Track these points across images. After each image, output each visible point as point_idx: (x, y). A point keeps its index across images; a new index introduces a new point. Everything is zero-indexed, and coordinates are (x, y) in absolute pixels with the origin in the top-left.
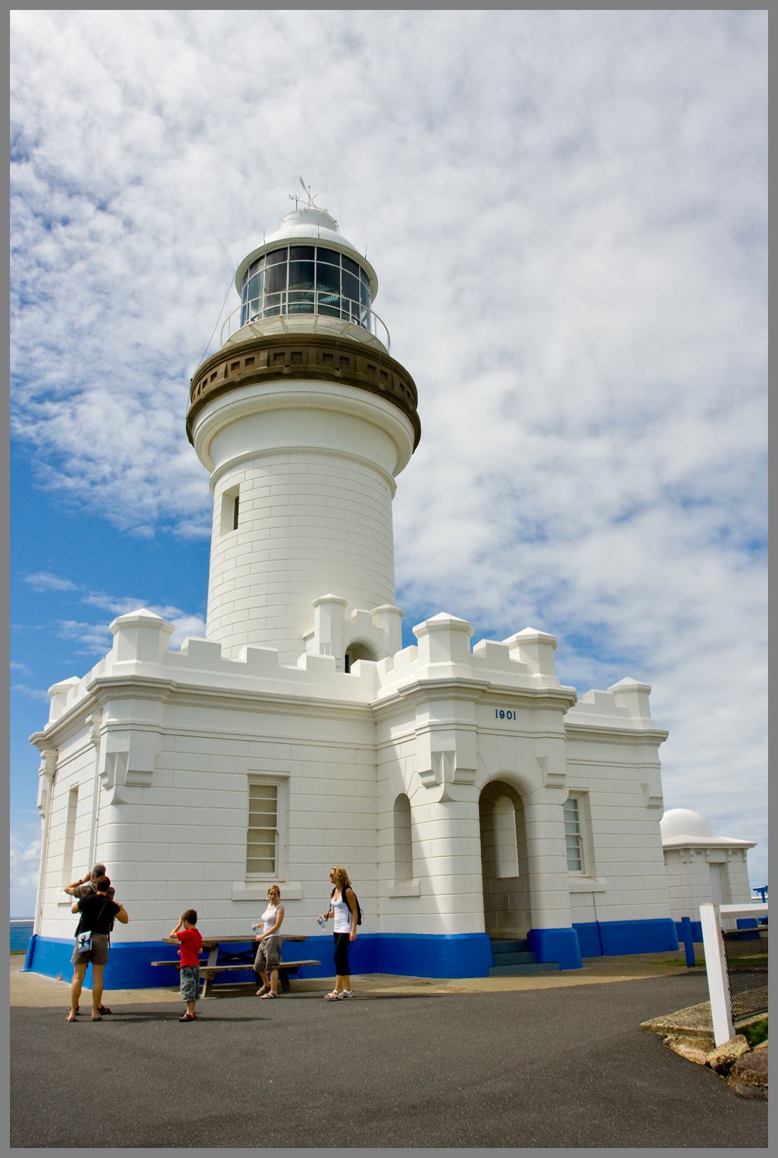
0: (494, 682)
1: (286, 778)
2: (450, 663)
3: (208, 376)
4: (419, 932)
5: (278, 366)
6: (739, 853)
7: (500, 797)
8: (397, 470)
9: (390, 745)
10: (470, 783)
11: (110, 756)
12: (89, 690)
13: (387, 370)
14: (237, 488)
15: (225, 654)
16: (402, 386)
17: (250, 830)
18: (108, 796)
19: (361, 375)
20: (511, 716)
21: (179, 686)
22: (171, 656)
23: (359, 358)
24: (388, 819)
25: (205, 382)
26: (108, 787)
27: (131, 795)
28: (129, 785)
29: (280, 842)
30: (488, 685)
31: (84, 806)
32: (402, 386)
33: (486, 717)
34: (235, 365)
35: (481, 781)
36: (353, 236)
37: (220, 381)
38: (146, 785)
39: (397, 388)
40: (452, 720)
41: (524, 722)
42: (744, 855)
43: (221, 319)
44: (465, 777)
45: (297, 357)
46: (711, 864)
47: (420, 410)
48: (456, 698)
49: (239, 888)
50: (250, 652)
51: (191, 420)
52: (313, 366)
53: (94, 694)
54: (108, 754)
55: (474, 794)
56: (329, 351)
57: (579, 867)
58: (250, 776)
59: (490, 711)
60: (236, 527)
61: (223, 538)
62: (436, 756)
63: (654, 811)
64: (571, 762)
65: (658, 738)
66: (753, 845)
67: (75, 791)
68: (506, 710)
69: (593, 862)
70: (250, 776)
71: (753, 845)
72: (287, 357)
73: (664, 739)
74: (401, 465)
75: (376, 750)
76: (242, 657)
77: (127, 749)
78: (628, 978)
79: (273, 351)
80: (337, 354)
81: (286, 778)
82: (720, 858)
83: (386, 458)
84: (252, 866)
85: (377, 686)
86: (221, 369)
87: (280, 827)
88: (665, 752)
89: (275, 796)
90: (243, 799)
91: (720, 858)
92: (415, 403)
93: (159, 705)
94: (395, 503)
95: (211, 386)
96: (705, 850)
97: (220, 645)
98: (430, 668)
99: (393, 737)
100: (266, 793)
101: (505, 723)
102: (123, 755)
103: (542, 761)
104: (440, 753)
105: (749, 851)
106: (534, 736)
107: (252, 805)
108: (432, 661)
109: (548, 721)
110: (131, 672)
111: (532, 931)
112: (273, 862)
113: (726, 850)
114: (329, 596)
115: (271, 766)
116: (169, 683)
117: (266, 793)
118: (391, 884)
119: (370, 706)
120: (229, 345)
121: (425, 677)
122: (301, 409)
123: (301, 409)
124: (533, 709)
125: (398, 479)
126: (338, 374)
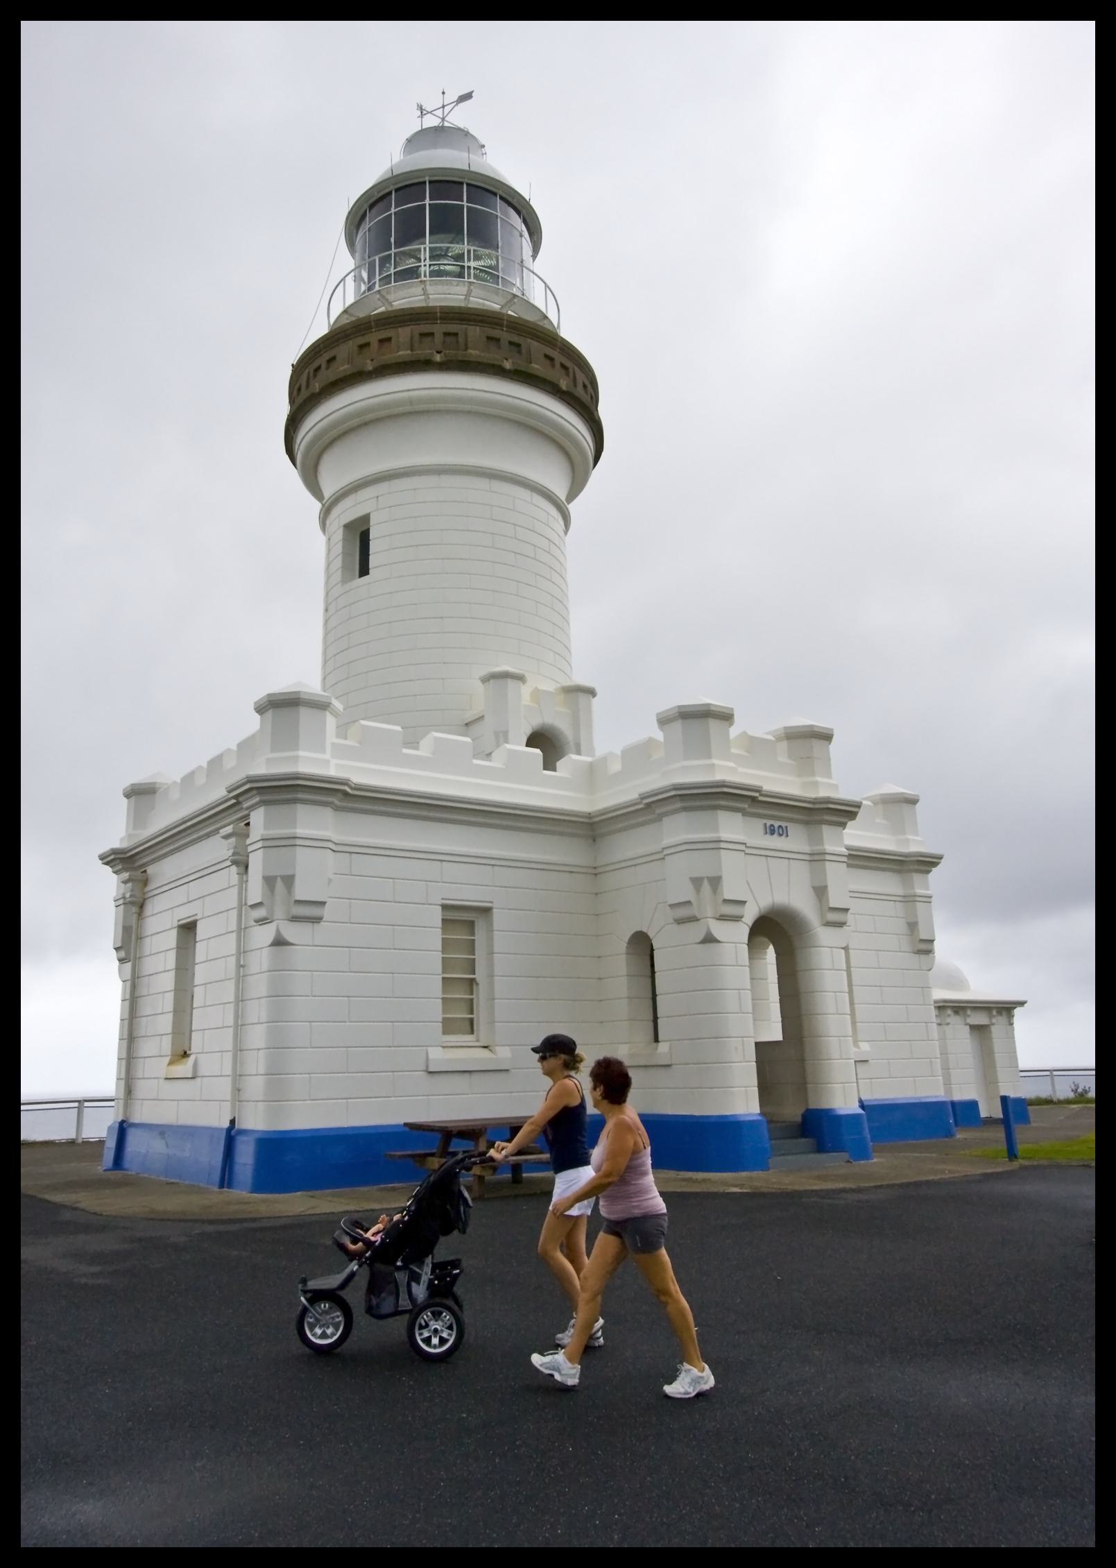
0: (767, 787)
1: (486, 911)
3: (322, 361)
5: (423, 352)
6: (1004, 1013)
8: (573, 493)
10: (737, 918)
12: (229, 792)
13: (568, 364)
14: (365, 519)
16: (585, 386)
17: (443, 978)
19: (537, 368)
20: (782, 832)
21: (359, 788)
24: (619, 964)
25: (317, 369)
26: (262, 921)
30: (758, 790)
31: (214, 947)
32: (585, 386)
35: (750, 914)
39: (566, 376)
42: (1010, 1016)
43: (322, 285)
45: (449, 339)
47: (605, 411)
48: (685, 809)
49: (437, 1056)
52: (474, 353)
53: (236, 797)
55: (743, 931)
56: (425, 328)
57: (471, 1027)
59: (758, 824)
60: (364, 570)
61: (348, 586)
63: (923, 957)
64: (856, 895)
65: (927, 863)
66: (1022, 1004)
67: (188, 929)
68: (777, 824)
69: (492, 1022)
71: (1022, 1004)
72: (439, 338)
73: (935, 864)
75: (595, 872)
78: (534, 1175)
80: (505, 336)
81: (941, 858)
82: (980, 1019)
83: (555, 479)
84: (449, 1026)
87: (480, 975)
89: (473, 934)
90: (435, 937)
91: (980, 1019)
92: (595, 399)
95: (328, 375)
96: (964, 1008)
101: (775, 842)
105: (1017, 1012)
107: (446, 945)
108: (273, 750)
111: (808, 1111)
112: (471, 1021)
116: (345, 782)
119: (589, 816)
120: (346, 320)
122: (448, 412)
123: (448, 412)
126: (508, 365)
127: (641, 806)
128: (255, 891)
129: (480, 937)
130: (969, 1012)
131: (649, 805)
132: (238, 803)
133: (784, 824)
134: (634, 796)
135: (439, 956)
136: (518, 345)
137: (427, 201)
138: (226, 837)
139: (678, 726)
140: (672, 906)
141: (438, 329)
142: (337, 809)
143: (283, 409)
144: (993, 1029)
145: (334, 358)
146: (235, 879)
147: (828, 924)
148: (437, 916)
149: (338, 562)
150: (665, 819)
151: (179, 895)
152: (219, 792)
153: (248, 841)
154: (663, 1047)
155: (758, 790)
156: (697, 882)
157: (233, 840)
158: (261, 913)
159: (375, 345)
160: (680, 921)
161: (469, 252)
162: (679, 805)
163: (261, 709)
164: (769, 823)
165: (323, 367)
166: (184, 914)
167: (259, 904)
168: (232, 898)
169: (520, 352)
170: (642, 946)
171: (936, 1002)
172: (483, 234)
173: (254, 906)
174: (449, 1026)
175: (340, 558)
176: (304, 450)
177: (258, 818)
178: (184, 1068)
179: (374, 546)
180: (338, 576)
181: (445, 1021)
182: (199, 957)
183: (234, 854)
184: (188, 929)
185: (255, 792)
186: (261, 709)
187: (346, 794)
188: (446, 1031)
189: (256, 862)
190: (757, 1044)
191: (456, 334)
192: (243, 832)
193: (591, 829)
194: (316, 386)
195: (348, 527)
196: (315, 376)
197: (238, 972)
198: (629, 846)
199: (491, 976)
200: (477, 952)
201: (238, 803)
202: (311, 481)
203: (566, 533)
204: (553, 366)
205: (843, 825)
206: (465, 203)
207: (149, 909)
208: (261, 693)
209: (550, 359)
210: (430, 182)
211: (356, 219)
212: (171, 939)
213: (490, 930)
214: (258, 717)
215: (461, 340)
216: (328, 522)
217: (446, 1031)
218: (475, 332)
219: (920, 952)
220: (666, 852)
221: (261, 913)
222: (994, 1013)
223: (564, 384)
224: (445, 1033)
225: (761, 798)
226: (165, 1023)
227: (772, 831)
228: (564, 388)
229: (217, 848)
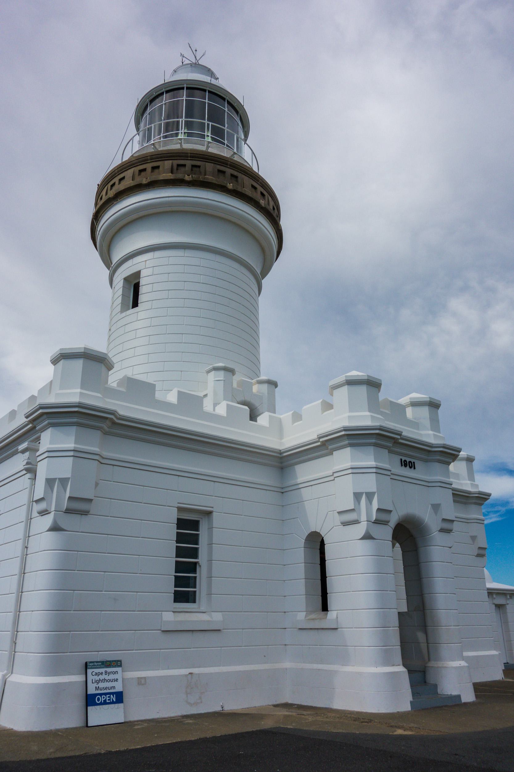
1: (209, 514)
2: (368, 413)
7: (408, 536)
9: (296, 488)
11: (50, 482)
14: (137, 275)
15: (158, 395)
16: (274, 209)
20: (412, 466)
22: (110, 392)
23: (246, 178)
25: (113, 185)
26: (43, 513)
27: (66, 521)
35: (394, 520)
37: (128, 183)
38: (85, 513)
40: (373, 463)
44: (383, 517)
45: (195, 169)
47: (284, 223)
48: (376, 445)
50: (181, 394)
51: (97, 217)
52: (210, 178)
55: (387, 532)
58: (180, 509)
60: (135, 304)
61: (124, 314)
62: (357, 496)
69: (210, 594)
70: (180, 509)
72: (188, 168)
74: (266, 269)
76: (172, 398)
77: (68, 475)
79: (176, 162)
81: (209, 514)
85: (281, 436)
86: (129, 174)
90: (172, 531)
93: (98, 433)
94: (262, 300)
97: (154, 386)
98: (349, 417)
99: (300, 480)
100: (189, 529)
101: (407, 472)
103: (436, 507)
104: (361, 494)
106: (428, 484)
108: (350, 411)
110: (75, 399)
114: (221, 364)
115: (196, 497)
117: (189, 529)
118: (301, 616)
119: (280, 452)
121: (347, 424)
125: (264, 282)
127: (319, 444)
129: (203, 533)
130: (494, 596)
132: (34, 428)
133: (412, 461)
134: (314, 437)
136: (236, 177)
140: (339, 513)
141: (189, 163)
142: (106, 433)
143: (91, 210)
145: (123, 178)
148: (174, 516)
149: (119, 300)
150: (334, 453)
152: (21, 420)
153: (38, 454)
154: (332, 615)
155: (399, 434)
157: (27, 454)
158: (43, 506)
159: (149, 170)
160: (345, 524)
161: (208, 124)
162: (347, 442)
163: (55, 361)
164: (404, 459)
165: (117, 183)
167: (42, 499)
168: (24, 498)
169: (237, 181)
171: (488, 589)
172: (216, 116)
173: (37, 501)
174: (180, 597)
175: (121, 289)
176: (104, 240)
179: (142, 290)
180: (119, 308)
181: (176, 593)
183: (28, 463)
185: (45, 416)
186: (55, 361)
187: (114, 423)
188: (176, 600)
190: (399, 613)
191: (199, 167)
194: (111, 194)
195: (126, 279)
196: (111, 189)
197: (23, 552)
198: (305, 473)
199: (210, 561)
200: (200, 543)
201: (35, 427)
202: (106, 259)
203: (259, 294)
204: (256, 192)
205: (449, 464)
206: (207, 101)
208: (55, 350)
209: (255, 188)
210: (187, 88)
211: (142, 110)
213: (211, 528)
214: (52, 367)
215: (202, 169)
216: (114, 279)
217: (176, 600)
218: (209, 167)
219: (479, 555)
220: (335, 475)
221: (43, 506)
222: (508, 597)
223: (262, 202)
225: (401, 441)
227: (404, 464)
228: (263, 205)
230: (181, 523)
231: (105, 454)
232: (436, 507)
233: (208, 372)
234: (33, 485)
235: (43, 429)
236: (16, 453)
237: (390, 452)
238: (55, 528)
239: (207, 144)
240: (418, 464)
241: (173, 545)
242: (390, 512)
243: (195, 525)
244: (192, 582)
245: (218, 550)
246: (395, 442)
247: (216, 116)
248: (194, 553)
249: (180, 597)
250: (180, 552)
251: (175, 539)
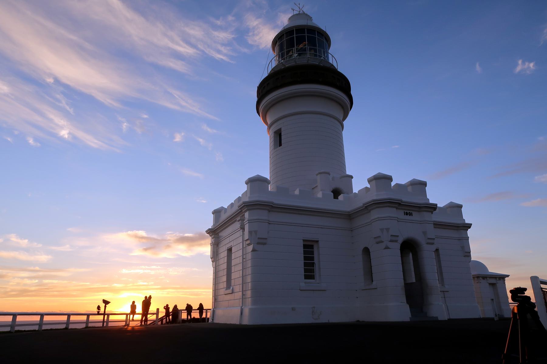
0: (404, 200)
1: (317, 241)
4: (334, 322)
7: (409, 247)
8: (344, 119)
10: (396, 241)
11: (250, 232)
18: (250, 248)
20: (411, 214)
25: (264, 88)
26: (249, 245)
28: (258, 243)
29: (316, 267)
30: (401, 201)
33: (400, 214)
34: (264, 88)
35: (401, 240)
36: (319, 22)
38: (265, 244)
39: (343, 84)
41: (416, 216)
44: (394, 238)
46: (490, 284)
47: (352, 92)
53: (240, 209)
54: (249, 232)
55: (398, 246)
58: (304, 240)
59: (402, 212)
66: (508, 276)
67: (230, 250)
68: (408, 212)
70: (304, 240)
71: (508, 276)
73: (470, 227)
76: (297, 192)
88: (469, 232)
90: (302, 250)
91: (493, 281)
96: (486, 277)
100: (309, 248)
101: (408, 217)
102: (256, 232)
103: (425, 233)
105: (506, 279)
109: (427, 216)
113: (496, 278)
115: (311, 235)
117: (309, 248)
119: (349, 212)
120: (273, 71)
121: (375, 198)
124: (419, 211)
125: (345, 123)
128: (246, 237)
131: (366, 207)
135: (302, 256)
137: (295, 35)
138: (238, 221)
139: (374, 182)
143: (256, 99)
144: (497, 284)
146: (241, 233)
147: (428, 243)
148: (302, 243)
151: (227, 241)
152: (236, 208)
154: (374, 283)
156: (382, 230)
160: (377, 243)
166: (228, 246)
170: (366, 251)
172: (312, 42)
173: (246, 240)
174: (307, 277)
177: (247, 215)
178: (230, 291)
182: (233, 257)
184: (230, 250)
189: (247, 227)
192: (243, 220)
193: (350, 216)
201: (242, 211)
207: (220, 246)
212: (225, 253)
221: (248, 242)
224: (305, 279)
226: (224, 279)
229: (237, 225)
230: (305, 246)
231: (150, 271)
232: (425, 233)
233: (317, 175)
234: (243, 234)
235: (245, 212)
236: (236, 221)
237: (397, 208)
238: (254, 250)
239: (308, 59)
240: (413, 213)
241: (302, 256)
242: (398, 236)
243: (312, 247)
244: (312, 271)
245: (322, 256)
246: (400, 204)
247: (312, 42)
248: (312, 259)
249: (307, 277)
250: (305, 259)
251: (451, 318)
